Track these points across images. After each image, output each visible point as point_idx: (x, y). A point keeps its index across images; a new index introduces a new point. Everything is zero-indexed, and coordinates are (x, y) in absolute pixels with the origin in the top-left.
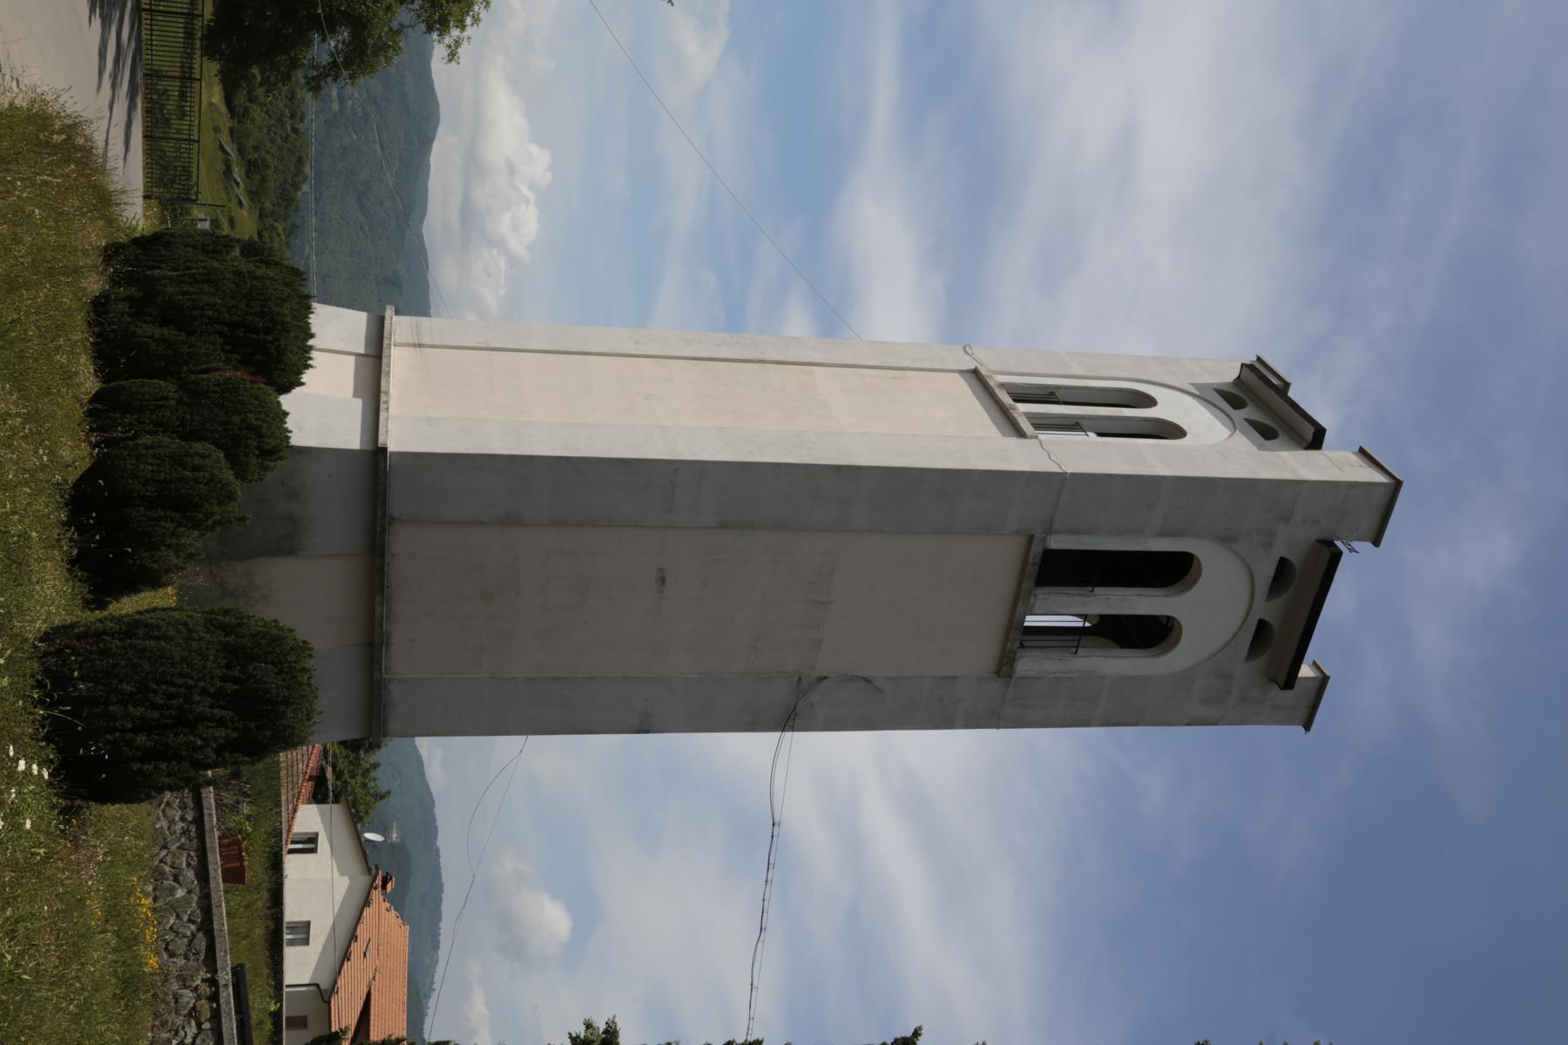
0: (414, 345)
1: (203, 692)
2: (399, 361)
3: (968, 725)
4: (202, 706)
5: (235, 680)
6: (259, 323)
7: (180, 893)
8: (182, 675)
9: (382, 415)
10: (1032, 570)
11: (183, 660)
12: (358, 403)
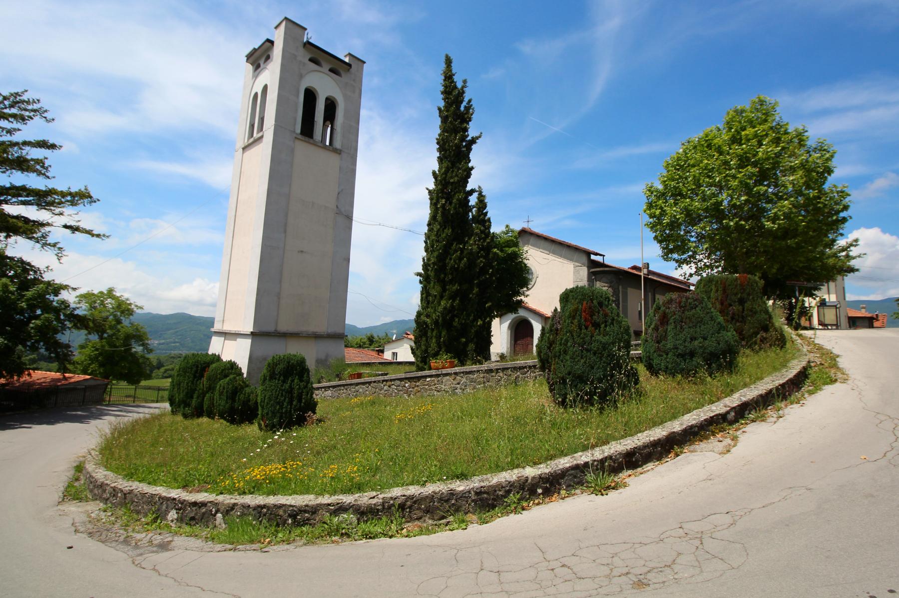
0: (223, 323)
1: (282, 386)
2: (227, 328)
3: (355, 165)
4: (287, 386)
5: (280, 377)
6: (195, 369)
7: (361, 390)
8: (276, 391)
9: (242, 333)
10: (307, 139)
11: (271, 392)
12: (238, 340)
